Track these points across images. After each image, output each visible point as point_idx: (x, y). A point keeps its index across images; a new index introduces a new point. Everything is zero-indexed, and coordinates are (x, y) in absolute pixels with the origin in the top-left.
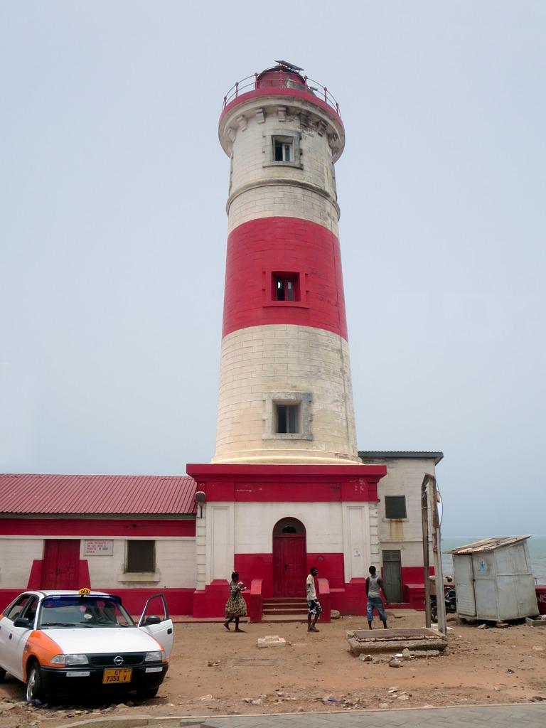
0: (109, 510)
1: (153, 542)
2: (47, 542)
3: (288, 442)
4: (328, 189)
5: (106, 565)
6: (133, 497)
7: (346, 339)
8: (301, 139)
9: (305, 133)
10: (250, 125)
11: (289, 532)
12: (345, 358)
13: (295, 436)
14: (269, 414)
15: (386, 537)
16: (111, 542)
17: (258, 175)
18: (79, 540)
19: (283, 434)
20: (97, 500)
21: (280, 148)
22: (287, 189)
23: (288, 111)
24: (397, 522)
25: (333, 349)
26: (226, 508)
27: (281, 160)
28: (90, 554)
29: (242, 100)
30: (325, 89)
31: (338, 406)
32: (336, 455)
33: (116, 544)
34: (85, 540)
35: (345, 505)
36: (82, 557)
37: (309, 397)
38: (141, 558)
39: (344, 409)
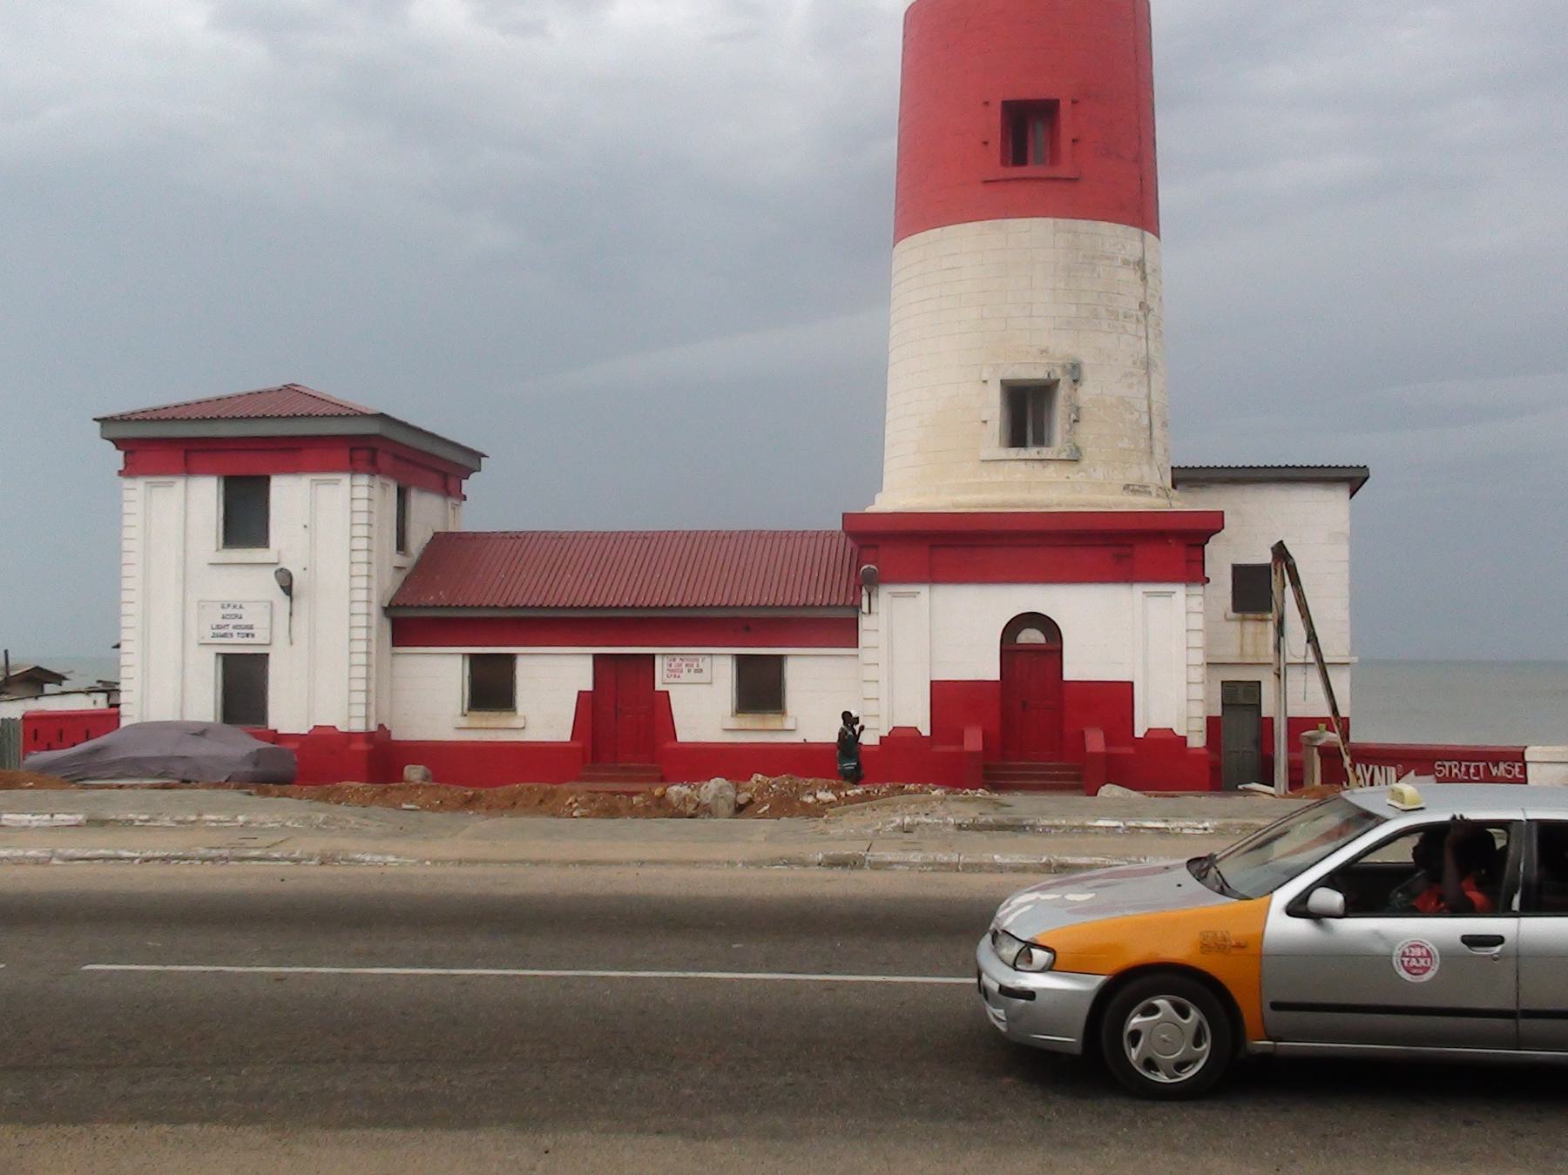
1: (780, 659)
5: (700, 696)
7: (1158, 236)
11: (1031, 650)
13: (1046, 453)
14: (993, 407)
15: (1230, 653)
16: (708, 659)
18: (653, 656)
26: (914, 595)
28: (672, 680)
31: (1130, 386)
32: (1126, 487)
33: (716, 660)
35: (1139, 589)
36: (659, 686)
37: (1075, 372)
38: (760, 689)
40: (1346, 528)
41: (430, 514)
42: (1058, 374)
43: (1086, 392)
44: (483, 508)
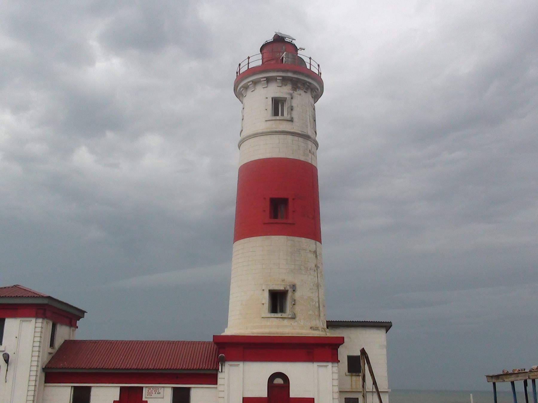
0: (163, 366)
2: (121, 388)
3: (278, 319)
4: (310, 133)
6: (164, 360)
8: (292, 98)
9: (295, 94)
10: (256, 88)
12: (318, 257)
13: (284, 315)
14: (266, 298)
16: (162, 389)
17: (262, 126)
18: (142, 388)
19: (276, 314)
20: (120, 359)
21: (277, 105)
22: (282, 136)
23: (285, 80)
24: (356, 375)
25: (310, 251)
26: (326, 366)
27: (278, 115)
28: (149, 396)
29: (252, 71)
30: (319, 66)
31: (312, 293)
32: (311, 328)
34: (146, 387)
35: (316, 364)
36: (144, 399)
37: (294, 288)
39: (317, 294)
40: (385, 343)
41: (64, 333)
42: (288, 288)
43: (298, 295)
44: (84, 331)
